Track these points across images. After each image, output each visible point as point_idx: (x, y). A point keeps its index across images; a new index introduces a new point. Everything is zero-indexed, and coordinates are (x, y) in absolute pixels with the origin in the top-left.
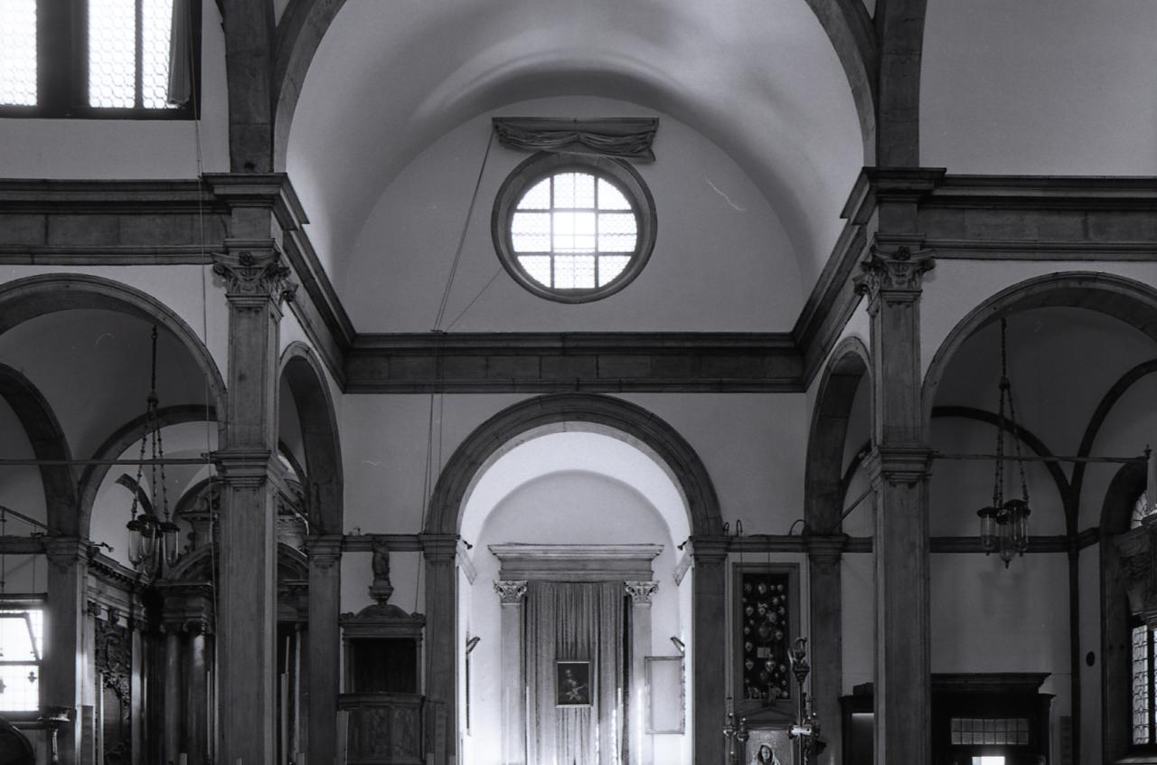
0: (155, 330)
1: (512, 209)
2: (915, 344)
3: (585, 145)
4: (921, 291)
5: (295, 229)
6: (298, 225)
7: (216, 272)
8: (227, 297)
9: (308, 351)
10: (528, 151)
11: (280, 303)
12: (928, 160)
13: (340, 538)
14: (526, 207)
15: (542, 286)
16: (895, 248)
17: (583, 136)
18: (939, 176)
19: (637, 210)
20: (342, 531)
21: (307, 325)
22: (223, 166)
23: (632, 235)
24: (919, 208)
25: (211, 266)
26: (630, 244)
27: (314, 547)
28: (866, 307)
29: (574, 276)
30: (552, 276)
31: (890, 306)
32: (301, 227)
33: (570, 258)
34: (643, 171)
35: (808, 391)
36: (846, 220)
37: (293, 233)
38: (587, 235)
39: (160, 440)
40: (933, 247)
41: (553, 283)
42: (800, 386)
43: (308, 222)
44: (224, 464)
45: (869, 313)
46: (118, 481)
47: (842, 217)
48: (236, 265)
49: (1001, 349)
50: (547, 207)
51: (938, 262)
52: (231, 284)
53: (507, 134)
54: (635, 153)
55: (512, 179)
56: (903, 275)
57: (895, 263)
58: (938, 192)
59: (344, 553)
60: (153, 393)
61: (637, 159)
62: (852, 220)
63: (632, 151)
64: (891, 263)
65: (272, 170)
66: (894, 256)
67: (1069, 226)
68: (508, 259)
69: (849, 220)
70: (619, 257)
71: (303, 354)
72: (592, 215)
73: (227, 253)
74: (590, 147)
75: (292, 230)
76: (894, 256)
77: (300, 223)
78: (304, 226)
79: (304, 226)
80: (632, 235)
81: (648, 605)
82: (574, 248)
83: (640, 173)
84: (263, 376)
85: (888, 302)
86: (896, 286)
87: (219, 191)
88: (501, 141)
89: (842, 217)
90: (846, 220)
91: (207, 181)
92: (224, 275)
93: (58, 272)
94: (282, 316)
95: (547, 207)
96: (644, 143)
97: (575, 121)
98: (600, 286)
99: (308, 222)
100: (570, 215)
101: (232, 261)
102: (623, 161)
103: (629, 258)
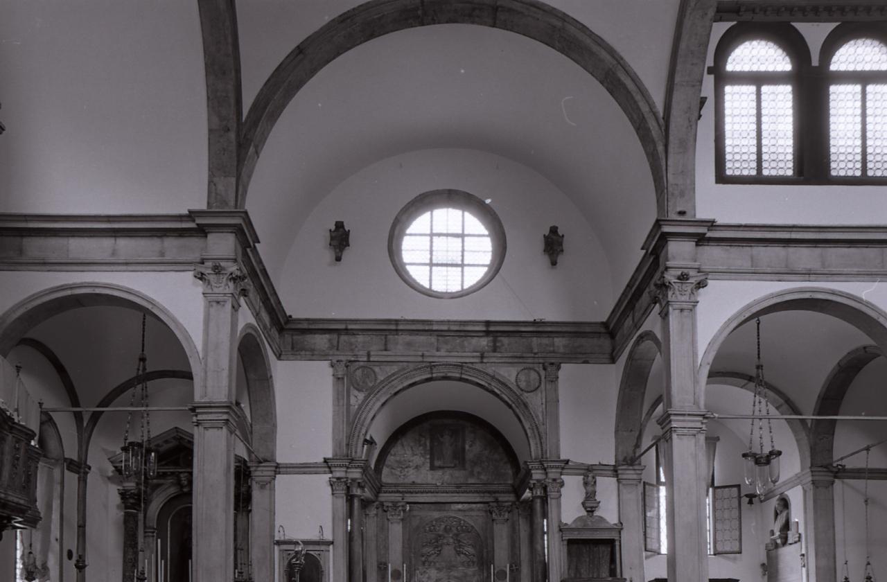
0: (144, 316)
1: (402, 234)
2: (693, 343)
4: (698, 302)
5: (250, 247)
6: (252, 244)
7: (195, 277)
8: (204, 294)
9: (256, 331)
11: (239, 298)
12: (702, 214)
13: (275, 465)
14: (413, 232)
16: (679, 273)
18: (711, 224)
20: (273, 454)
21: (257, 316)
22: (202, 205)
23: (488, 252)
24: (697, 245)
25: (193, 272)
27: (255, 471)
28: (659, 311)
29: (447, 282)
30: (431, 280)
32: (255, 247)
35: (617, 363)
36: (644, 251)
37: (248, 250)
38: (432, 226)
39: (146, 387)
40: (707, 273)
41: (431, 285)
42: (613, 360)
43: (259, 242)
44: (197, 411)
45: (661, 316)
47: (642, 249)
48: (210, 271)
49: (757, 340)
50: (435, 239)
51: (709, 281)
52: (207, 284)
58: (709, 234)
59: (277, 476)
60: (143, 354)
62: (649, 252)
65: (559, 458)
66: (679, 278)
67: (804, 257)
68: (399, 269)
69: (647, 252)
71: (253, 333)
73: (203, 263)
75: (248, 247)
76: (679, 278)
77: (254, 242)
78: (257, 245)
79: (257, 245)
80: (488, 252)
81: (564, 538)
84: (173, 320)
87: (200, 221)
89: (642, 249)
90: (644, 251)
91: (192, 215)
92: (201, 279)
93: (122, 297)
94: (240, 306)
95: (435, 239)
99: (259, 242)
101: (207, 269)
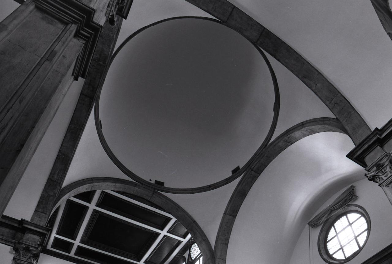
3: (335, 210)
10: (319, 225)
15: (343, 260)
17: (332, 209)
19: (363, 215)
26: (365, 226)
31: (388, 187)
33: (349, 245)
34: (357, 203)
46: (144, 263)
53: (313, 225)
54: (350, 200)
55: (320, 235)
56: (386, 172)
57: (379, 171)
61: (352, 201)
63: (349, 200)
64: (378, 173)
70: (364, 233)
72: (350, 227)
74: (336, 210)
82: (349, 240)
83: (356, 204)
85: (386, 186)
86: (385, 178)
88: (312, 227)
91: (23, 221)
96: (351, 195)
97: (329, 206)
98: (361, 246)
100: (343, 231)
102: (348, 205)
103: (367, 231)
